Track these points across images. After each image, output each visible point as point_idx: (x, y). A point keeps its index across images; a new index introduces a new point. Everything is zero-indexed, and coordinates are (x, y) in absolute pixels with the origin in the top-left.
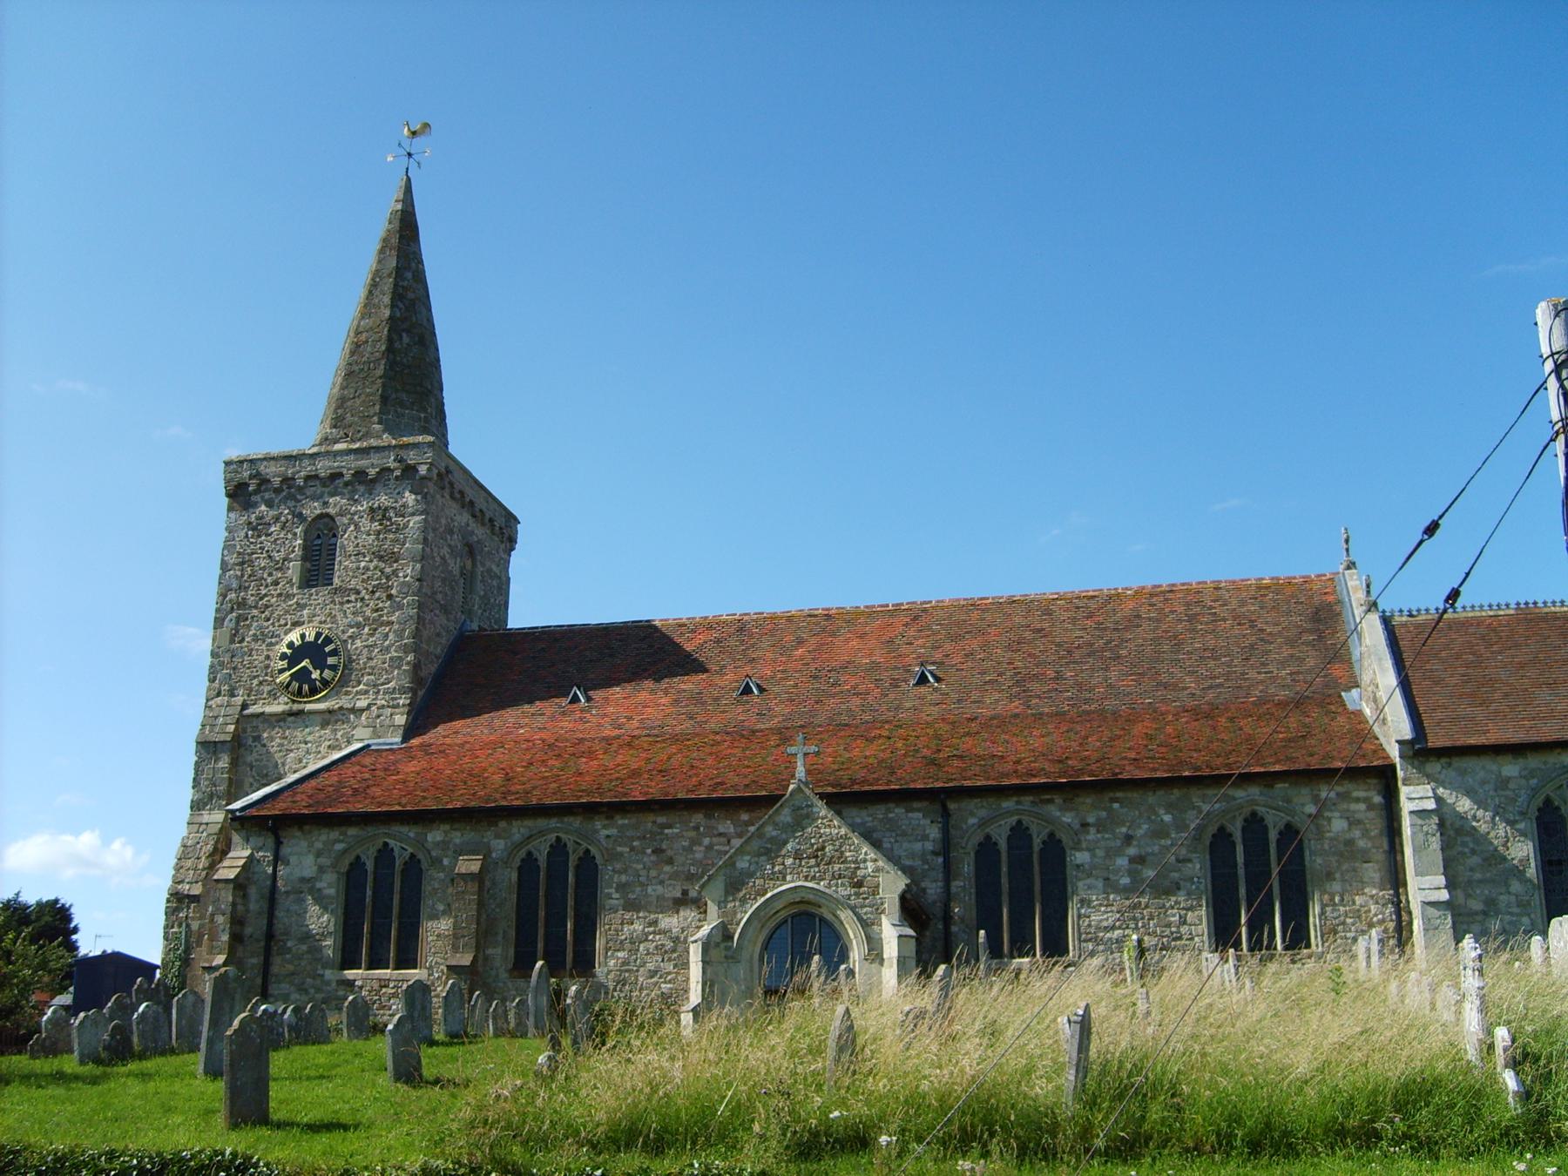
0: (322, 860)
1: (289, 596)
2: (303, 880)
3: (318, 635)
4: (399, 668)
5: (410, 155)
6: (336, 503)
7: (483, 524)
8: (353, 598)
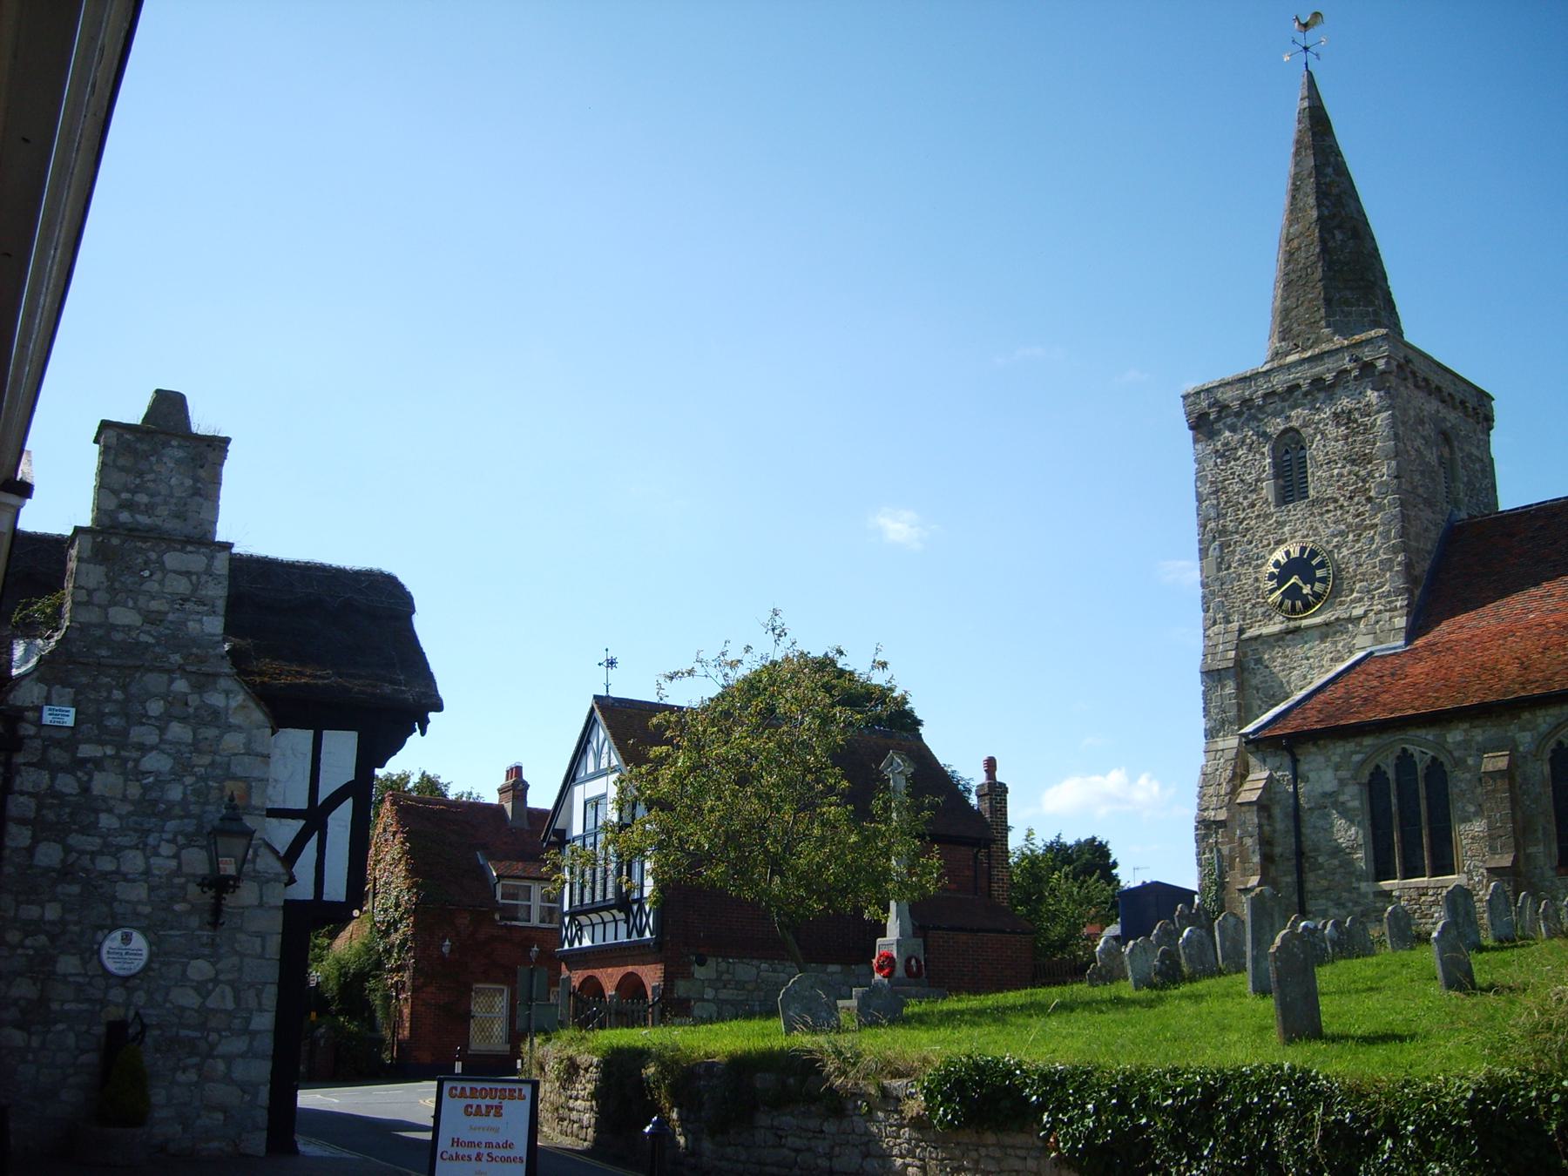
0: (1343, 774)
1: (1267, 516)
2: (1325, 795)
3: (1303, 549)
4: (1391, 570)
5: (1306, 49)
6: (1298, 416)
7: (1454, 408)
8: (1331, 507)
